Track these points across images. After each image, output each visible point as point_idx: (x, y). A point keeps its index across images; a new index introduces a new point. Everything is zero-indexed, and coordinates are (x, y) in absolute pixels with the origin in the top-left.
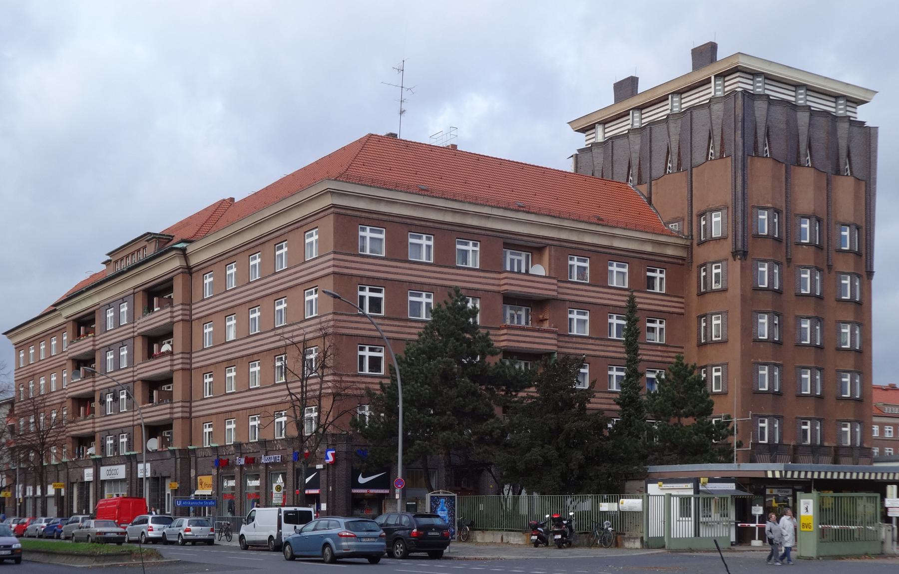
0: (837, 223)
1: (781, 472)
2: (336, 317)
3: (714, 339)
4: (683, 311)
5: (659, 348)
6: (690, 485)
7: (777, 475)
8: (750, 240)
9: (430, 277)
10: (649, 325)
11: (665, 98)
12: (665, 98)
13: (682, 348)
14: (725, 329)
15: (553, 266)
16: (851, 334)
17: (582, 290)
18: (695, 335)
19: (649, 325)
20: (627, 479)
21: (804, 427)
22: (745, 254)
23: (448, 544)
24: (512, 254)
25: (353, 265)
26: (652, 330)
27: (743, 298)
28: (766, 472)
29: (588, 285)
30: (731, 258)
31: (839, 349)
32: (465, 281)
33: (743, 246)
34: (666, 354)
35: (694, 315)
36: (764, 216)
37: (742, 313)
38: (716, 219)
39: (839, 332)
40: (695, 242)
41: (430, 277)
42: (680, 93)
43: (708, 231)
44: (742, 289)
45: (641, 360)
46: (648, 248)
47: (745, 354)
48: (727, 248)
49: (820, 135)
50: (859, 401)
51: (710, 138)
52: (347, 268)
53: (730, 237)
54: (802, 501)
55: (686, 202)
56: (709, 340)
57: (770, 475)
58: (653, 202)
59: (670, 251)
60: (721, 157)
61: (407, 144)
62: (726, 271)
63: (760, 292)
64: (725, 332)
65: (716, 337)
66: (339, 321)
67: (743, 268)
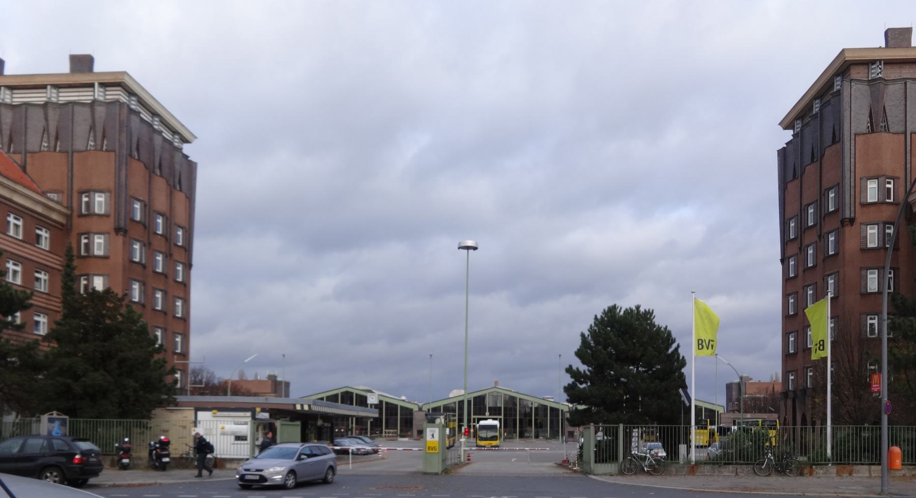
0: (175, 224)
6: (249, 414)
7: (306, 408)
11: (44, 87)
12: (44, 87)
20: (155, 407)
23: (100, 470)
26: (38, 279)
27: (124, 266)
28: (294, 405)
30: (113, 233)
31: (174, 317)
40: (75, 214)
42: (57, 87)
45: (32, 305)
46: (39, 209)
48: (109, 224)
49: (166, 156)
53: (112, 216)
57: (298, 407)
59: (55, 216)
60: (873, 131)
67: (124, 243)
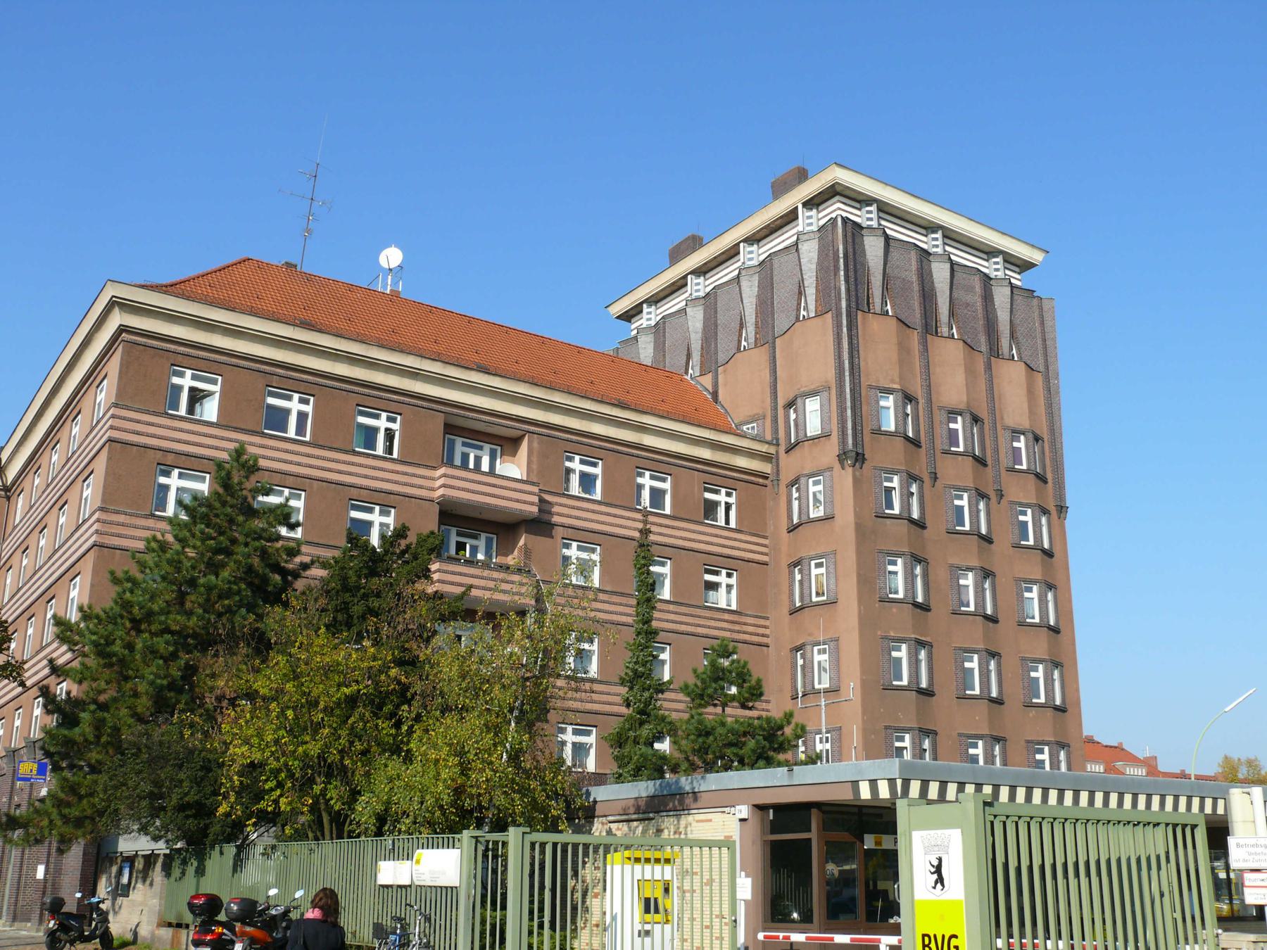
1: (892, 782)
2: (104, 516)
3: (815, 599)
4: (765, 559)
5: (726, 616)
8: (867, 437)
9: (299, 464)
10: (708, 577)
13: (767, 618)
14: (833, 581)
15: (534, 467)
16: (1040, 601)
17: (587, 510)
18: (785, 597)
19: (708, 577)
21: (957, 502)
22: (859, 458)
24: (464, 444)
25: (152, 430)
26: (713, 586)
27: (859, 527)
28: (855, 784)
29: (599, 503)
30: (837, 466)
31: (1022, 624)
32: (366, 477)
33: (855, 444)
34: (737, 627)
35: (784, 562)
36: (889, 402)
37: (859, 553)
38: (813, 406)
39: (1021, 598)
41: (299, 464)
43: (801, 427)
44: (857, 515)
47: (866, 623)
48: (833, 447)
50: (1061, 710)
51: (800, 293)
52: (138, 433)
54: (917, 836)
55: (768, 390)
56: (807, 601)
57: (865, 793)
58: (721, 398)
61: (309, 278)
62: (830, 491)
63: (888, 521)
64: (832, 586)
65: (818, 594)
66: (111, 523)
67: (857, 482)
